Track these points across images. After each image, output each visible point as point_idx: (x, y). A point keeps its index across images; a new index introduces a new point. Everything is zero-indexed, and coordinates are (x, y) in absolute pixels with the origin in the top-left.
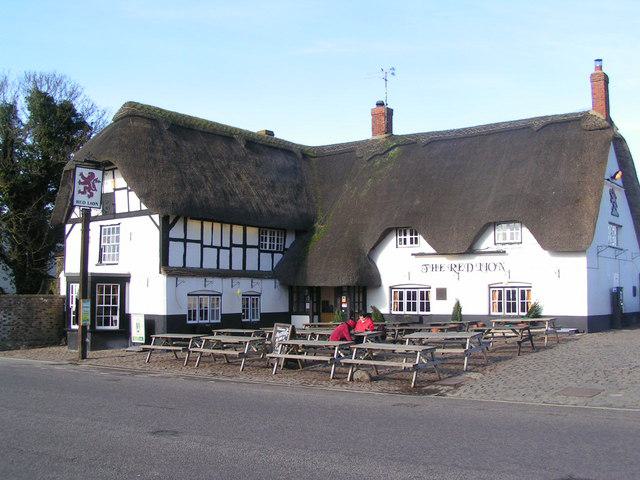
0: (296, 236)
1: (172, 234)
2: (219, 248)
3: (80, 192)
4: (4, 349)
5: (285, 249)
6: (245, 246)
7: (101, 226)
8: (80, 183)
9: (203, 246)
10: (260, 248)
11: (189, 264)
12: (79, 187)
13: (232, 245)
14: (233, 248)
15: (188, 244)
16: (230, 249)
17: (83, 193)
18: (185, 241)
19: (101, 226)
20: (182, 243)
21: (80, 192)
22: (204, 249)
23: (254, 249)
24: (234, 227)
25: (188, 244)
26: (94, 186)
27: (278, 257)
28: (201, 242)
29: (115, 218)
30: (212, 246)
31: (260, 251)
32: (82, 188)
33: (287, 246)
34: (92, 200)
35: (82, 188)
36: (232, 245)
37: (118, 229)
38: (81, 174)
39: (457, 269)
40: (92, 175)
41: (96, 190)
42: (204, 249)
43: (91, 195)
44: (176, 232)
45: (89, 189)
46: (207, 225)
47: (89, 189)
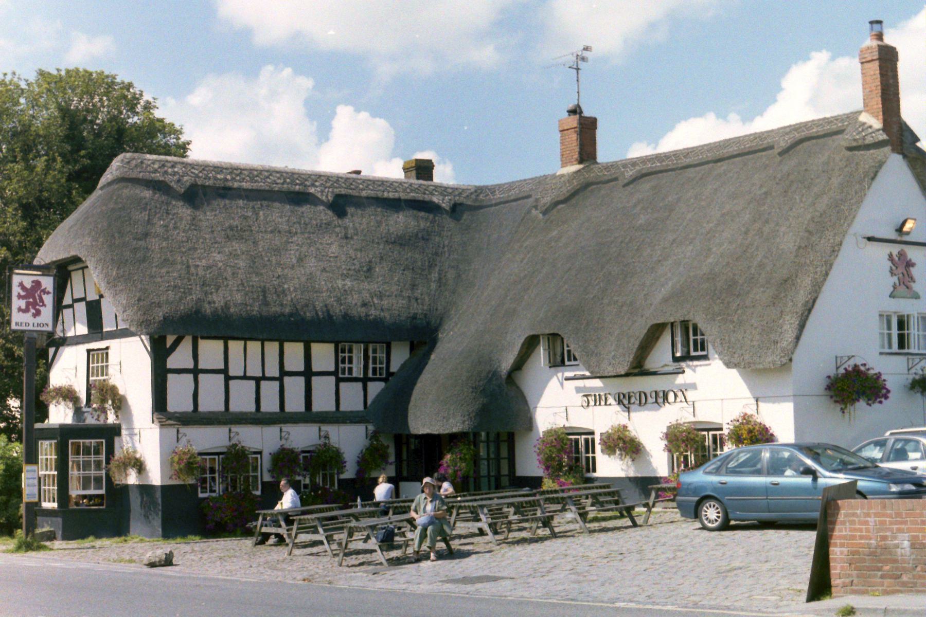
0: (412, 349)
1: (173, 361)
2: (258, 380)
3: (20, 310)
4: (925, 610)
5: (389, 374)
6: (308, 373)
7: (89, 351)
8: (19, 297)
9: (228, 378)
10: (340, 376)
11: (289, 408)
12: (17, 303)
13: (284, 373)
14: (277, 375)
15: (201, 377)
16: (280, 379)
17: (26, 311)
18: (196, 372)
19: (89, 351)
20: (190, 377)
21: (20, 310)
22: (231, 383)
23: (354, 384)
24: (249, 343)
25: (201, 377)
26: (42, 300)
27: (375, 388)
28: (225, 371)
29: (102, 339)
30: (245, 377)
31: (339, 381)
32: (23, 304)
33: (394, 368)
34: (39, 320)
35: (23, 304)
36: (283, 373)
37: (107, 354)
38: (21, 285)
39: (626, 402)
40: (37, 284)
41: (44, 305)
42: (231, 383)
43: (37, 313)
44: (180, 358)
45: (34, 304)
46: (236, 347)
47: (34, 304)
